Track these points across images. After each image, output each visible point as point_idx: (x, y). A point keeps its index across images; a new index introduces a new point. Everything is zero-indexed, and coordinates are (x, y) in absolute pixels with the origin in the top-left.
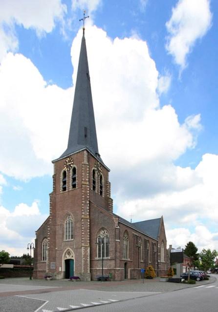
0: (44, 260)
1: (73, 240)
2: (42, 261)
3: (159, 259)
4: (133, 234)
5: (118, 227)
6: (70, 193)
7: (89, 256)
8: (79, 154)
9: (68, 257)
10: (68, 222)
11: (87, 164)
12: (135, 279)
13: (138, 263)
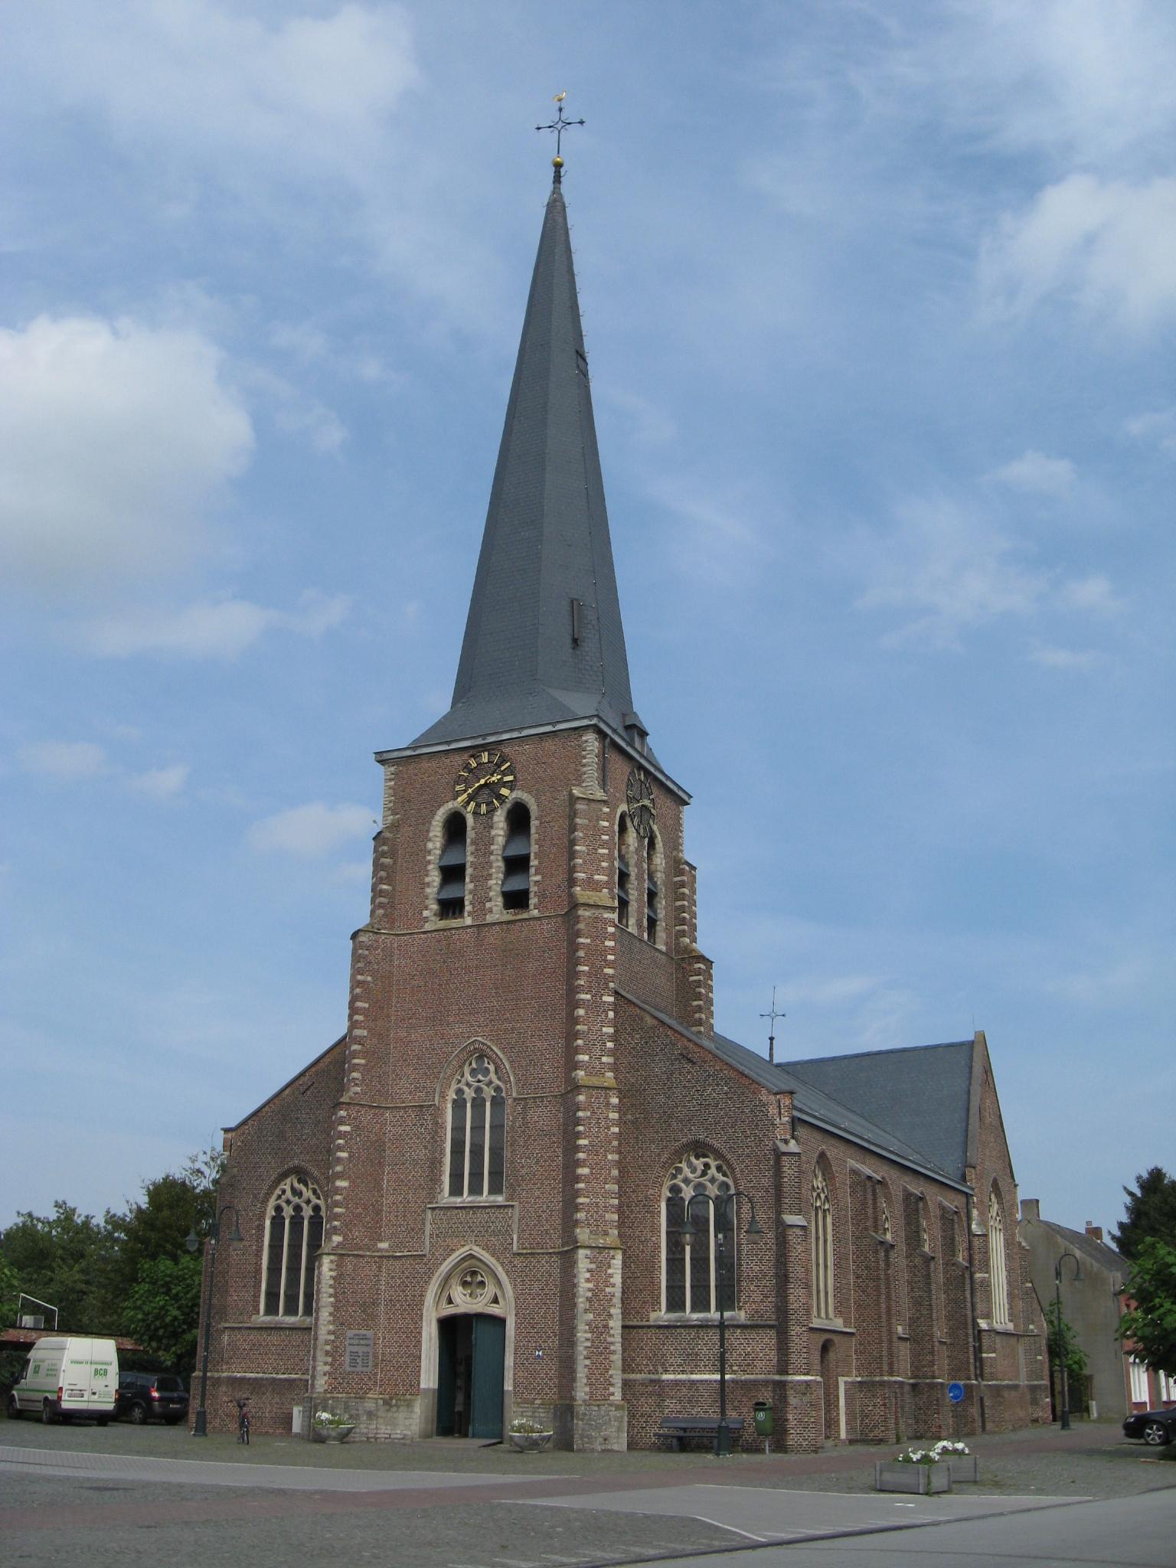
0: (291, 1310)
1: (500, 1199)
2: (262, 1318)
3: (980, 1307)
4: (854, 1172)
5: (793, 1147)
6: (492, 937)
7: (617, 1301)
8: (549, 745)
9: (464, 1302)
10: (469, 1094)
11: (600, 794)
12: (880, 1441)
13: (890, 1341)
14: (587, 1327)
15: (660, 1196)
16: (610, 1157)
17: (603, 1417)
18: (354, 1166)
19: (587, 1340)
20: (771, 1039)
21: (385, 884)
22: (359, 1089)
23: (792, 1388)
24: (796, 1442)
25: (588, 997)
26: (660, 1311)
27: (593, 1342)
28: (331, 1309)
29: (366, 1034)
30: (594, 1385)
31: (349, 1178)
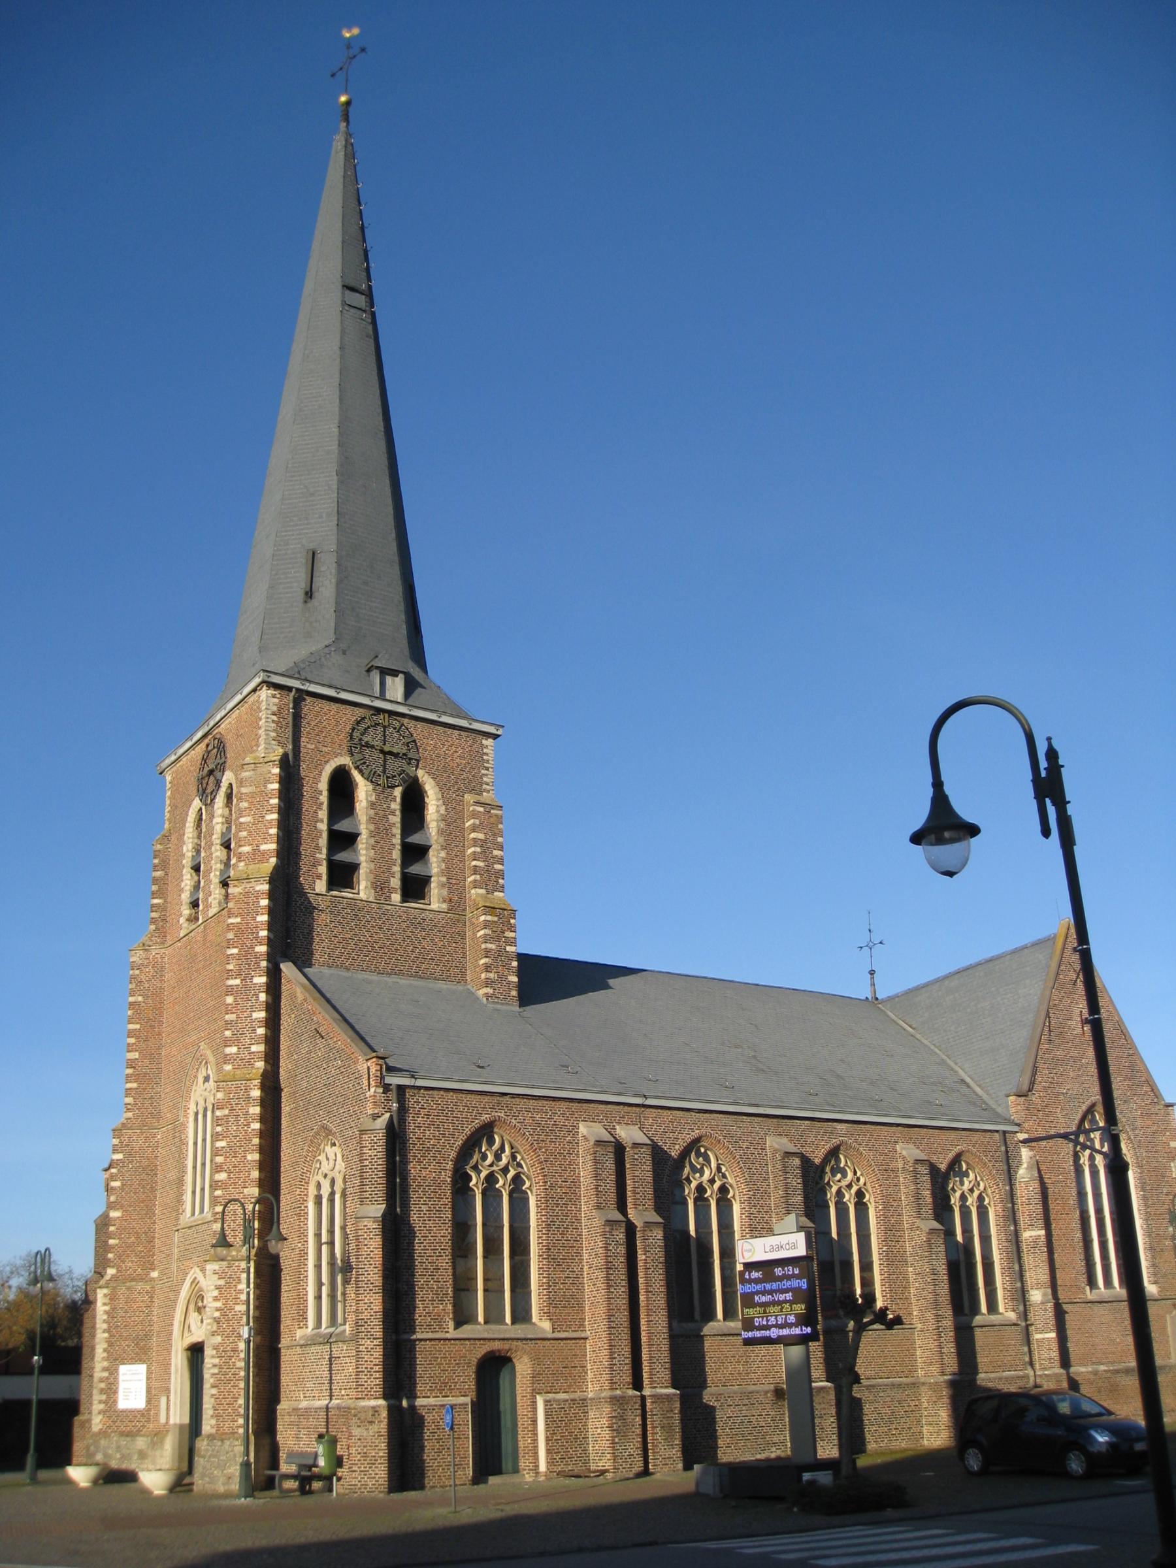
14: (215, 1352)
15: (306, 1195)
16: (249, 1157)
17: (227, 1453)
18: (126, 1194)
19: (215, 1366)
20: (872, 973)
21: (156, 898)
22: (131, 1114)
23: (355, 1416)
24: (359, 1481)
25: (237, 982)
26: (307, 1328)
27: (221, 1367)
28: (105, 1346)
29: (137, 1057)
30: (222, 1416)
31: (122, 1207)
